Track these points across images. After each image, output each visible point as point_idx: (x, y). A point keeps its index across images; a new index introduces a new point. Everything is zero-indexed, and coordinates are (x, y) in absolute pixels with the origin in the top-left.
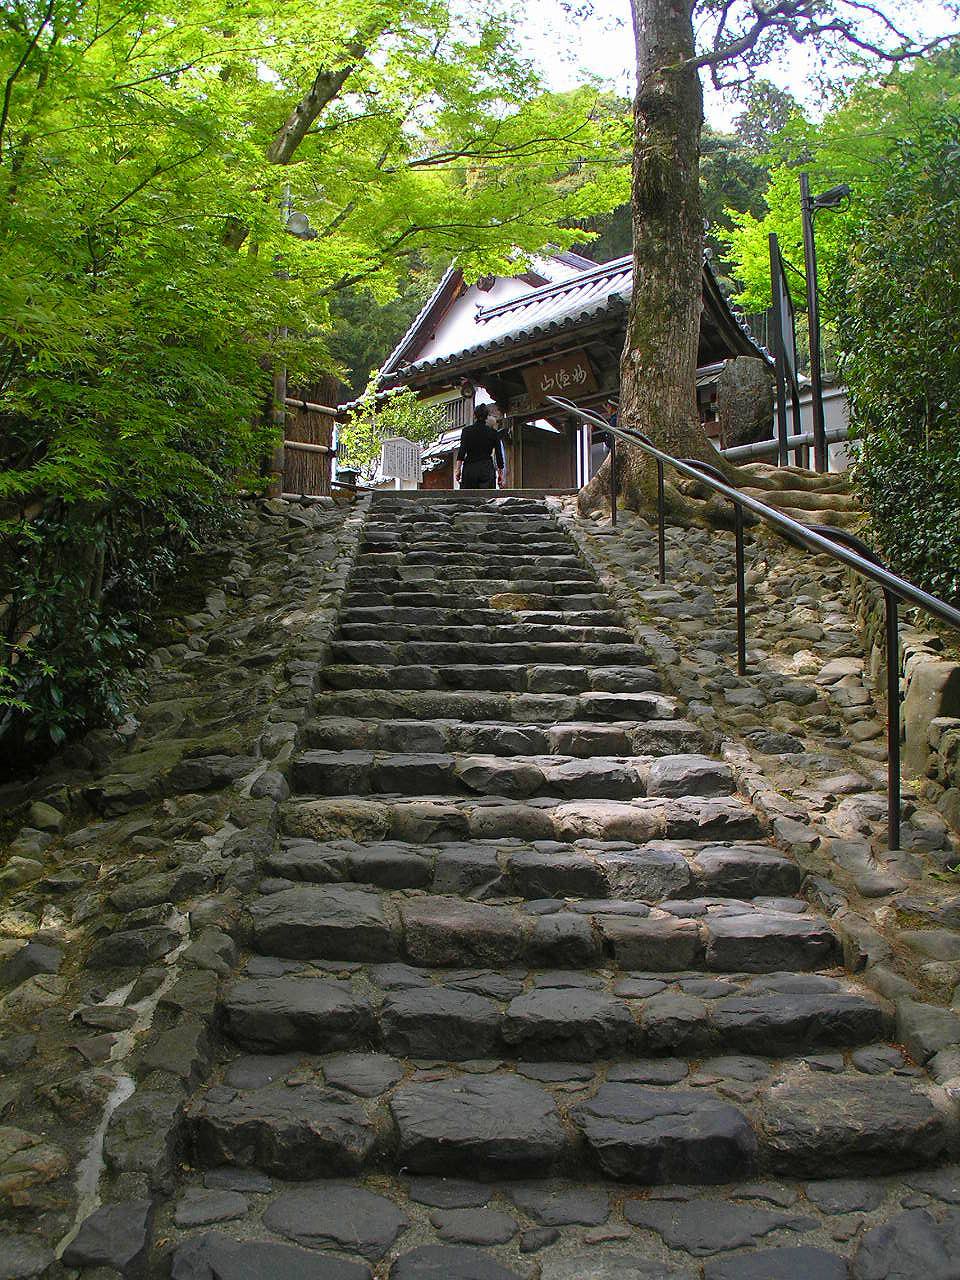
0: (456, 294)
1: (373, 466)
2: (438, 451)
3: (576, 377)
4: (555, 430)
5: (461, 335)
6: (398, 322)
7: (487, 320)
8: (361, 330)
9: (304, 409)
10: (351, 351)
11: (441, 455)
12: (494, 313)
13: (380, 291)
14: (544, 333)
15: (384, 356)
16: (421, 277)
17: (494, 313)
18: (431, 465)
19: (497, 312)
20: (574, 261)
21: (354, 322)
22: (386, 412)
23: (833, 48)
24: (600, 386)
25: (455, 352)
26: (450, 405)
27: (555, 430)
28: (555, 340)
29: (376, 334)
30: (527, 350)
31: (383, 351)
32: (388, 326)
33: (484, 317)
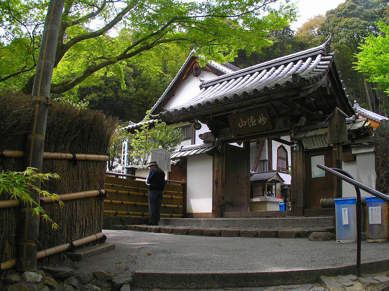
0: (184, 78)
1: (147, 155)
2: (179, 156)
3: (260, 121)
4: (230, 144)
5: (190, 95)
6: (159, 90)
7: (206, 88)
8: (147, 92)
9: (74, 161)
10: (143, 99)
11: (181, 158)
12: (210, 84)
13: (152, 69)
14: (249, 96)
15: (154, 101)
16: (168, 75)
17: (210, 84)
18: (175, 162)
19: (212, 84)
20: (231, 67)
21: (145, 90)
22: (153, 131)
23: (291, 14)
24: (274, 126)
25: (193, 104)
26: (183, 128)
27: (230, 144)
28: (254, 100)
29: (152, 93)
30: (235, 105)
31: (154, 99)
32: (156, 91)
33: (204, 86)
